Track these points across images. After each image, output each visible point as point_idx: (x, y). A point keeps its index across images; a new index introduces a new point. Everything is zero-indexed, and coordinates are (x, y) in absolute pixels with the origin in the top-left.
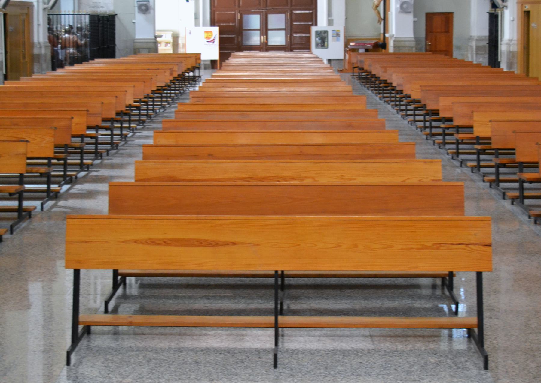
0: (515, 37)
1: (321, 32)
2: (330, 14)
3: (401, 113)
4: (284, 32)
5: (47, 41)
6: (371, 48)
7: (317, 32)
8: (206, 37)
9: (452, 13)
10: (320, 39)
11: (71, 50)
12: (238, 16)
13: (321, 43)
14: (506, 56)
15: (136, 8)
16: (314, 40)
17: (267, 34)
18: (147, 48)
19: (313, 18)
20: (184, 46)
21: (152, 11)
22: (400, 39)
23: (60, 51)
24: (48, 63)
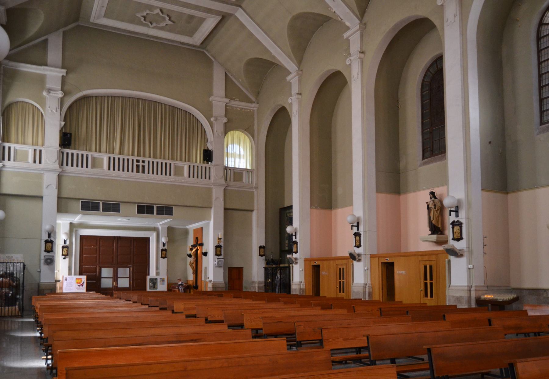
0: (303, 280)
1: (153, 279)
2: (157, 268)
7: (150, 279)
8: (77, 282)
9: (242, 268)
10: (152, 284)
12: (98, 269)
13: (153, 286)
17: (117, 281)
18: (50, 289)
19: (146, 271)
20: (61, 288)
21: (54, 263)
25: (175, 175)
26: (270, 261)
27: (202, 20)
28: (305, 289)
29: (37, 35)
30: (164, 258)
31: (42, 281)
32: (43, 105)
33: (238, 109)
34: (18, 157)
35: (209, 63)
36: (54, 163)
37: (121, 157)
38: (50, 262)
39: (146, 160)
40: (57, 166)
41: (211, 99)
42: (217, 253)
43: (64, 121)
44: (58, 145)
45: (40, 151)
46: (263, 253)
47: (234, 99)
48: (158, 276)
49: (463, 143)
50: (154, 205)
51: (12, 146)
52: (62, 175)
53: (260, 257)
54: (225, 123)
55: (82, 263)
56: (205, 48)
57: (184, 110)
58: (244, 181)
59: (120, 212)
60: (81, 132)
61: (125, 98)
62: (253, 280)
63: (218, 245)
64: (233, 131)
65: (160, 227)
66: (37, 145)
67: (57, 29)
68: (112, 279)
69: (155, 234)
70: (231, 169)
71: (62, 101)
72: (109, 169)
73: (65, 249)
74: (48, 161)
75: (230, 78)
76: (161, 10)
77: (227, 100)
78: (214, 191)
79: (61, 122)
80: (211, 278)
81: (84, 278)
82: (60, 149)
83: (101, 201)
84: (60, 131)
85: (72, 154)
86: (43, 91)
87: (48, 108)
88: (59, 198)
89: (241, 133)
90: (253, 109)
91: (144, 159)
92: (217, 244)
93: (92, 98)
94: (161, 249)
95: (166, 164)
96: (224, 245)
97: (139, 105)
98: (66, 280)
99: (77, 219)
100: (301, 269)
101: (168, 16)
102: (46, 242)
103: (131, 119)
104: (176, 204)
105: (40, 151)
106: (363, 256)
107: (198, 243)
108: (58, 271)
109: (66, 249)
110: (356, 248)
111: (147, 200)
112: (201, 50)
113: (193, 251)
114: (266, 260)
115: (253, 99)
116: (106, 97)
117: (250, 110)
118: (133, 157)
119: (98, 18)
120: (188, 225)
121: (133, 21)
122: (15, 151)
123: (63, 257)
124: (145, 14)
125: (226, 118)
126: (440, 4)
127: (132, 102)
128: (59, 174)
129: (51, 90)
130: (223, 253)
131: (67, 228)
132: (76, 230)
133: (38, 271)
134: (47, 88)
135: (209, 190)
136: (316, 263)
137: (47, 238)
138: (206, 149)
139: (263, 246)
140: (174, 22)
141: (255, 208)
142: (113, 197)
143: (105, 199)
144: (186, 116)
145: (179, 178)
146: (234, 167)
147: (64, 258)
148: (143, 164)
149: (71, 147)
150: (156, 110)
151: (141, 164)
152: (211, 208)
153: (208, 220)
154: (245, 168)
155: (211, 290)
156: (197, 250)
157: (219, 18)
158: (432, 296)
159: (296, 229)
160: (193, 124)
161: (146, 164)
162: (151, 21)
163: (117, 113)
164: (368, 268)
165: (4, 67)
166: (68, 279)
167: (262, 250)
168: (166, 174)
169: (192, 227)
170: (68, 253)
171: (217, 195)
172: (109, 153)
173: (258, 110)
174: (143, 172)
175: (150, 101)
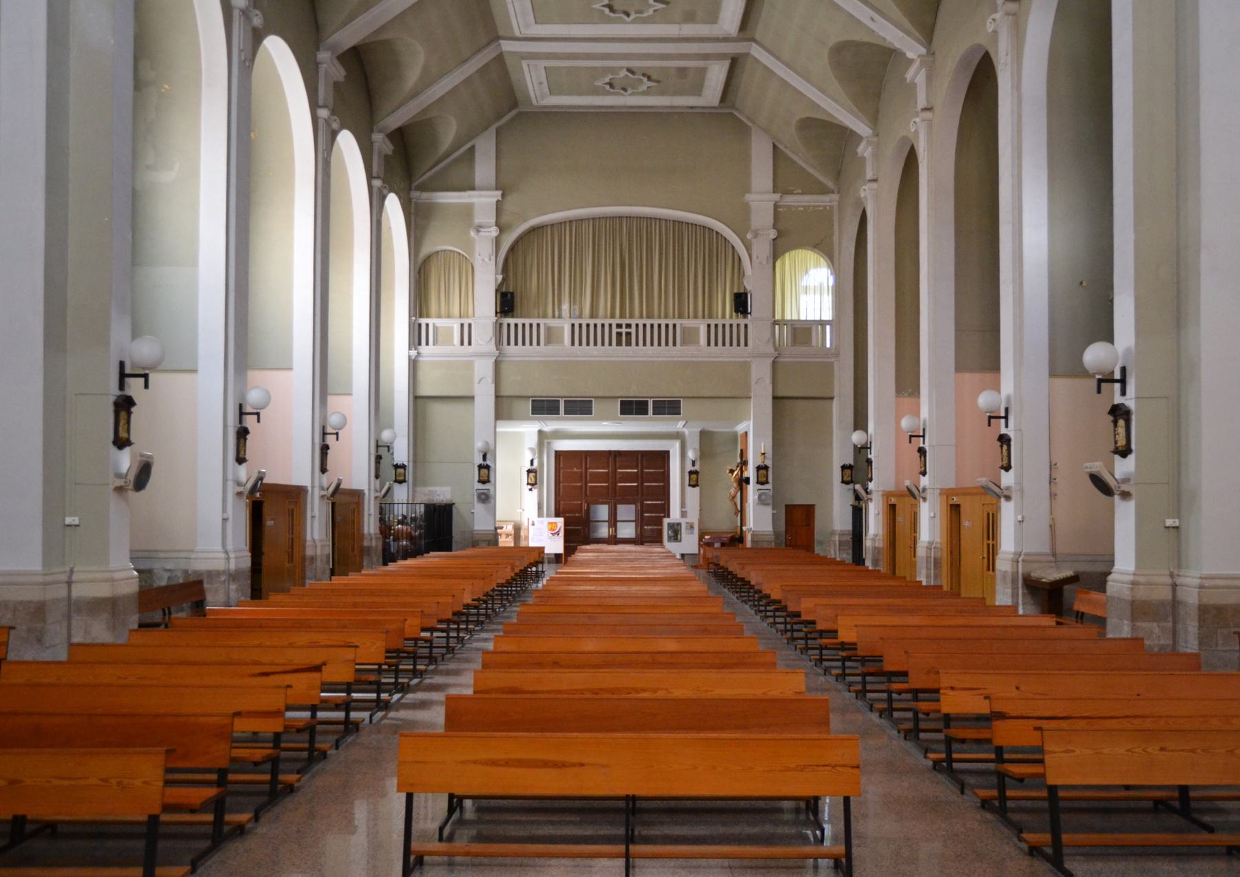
0: (881, 532)
1: (674, 524)
2: (683, 504)
5: (378, 531)
6: (728, 541)
7: (669, 524)
10: (672, 532)
11: (405, 543)
13: (674, 536)
14: (871, 552)
15: (476, 497)
16: (666, 533)
20: (527, 538)
21: (492, 501)
22: (758, 533)
25: (684, 343)
27: (702, 72)
29: (456, 146)
30: (694, 486)
32: (471, 252)
34: (440, 338)
35: (742, 131)
36: (488, 342)
37: (592, 322)
38: (486, 498)
39: (633, 322)
40: (492, 347)
41: (748, 197)
42: (760, 479)
45: (470, 325)
46: (849, 479)
47: (791, 193)
48: (683, 519)
50: (649, 399)
51: (430, 321)
52: (501, 361)
53: (844, 485)
54: (774, 240)
55: (559, 496)
57: (700, 226)
60: (530, 286)
63: (761, 464)
64: (793, 251)
66: (468, 317)
67: (486, 128)
68: (634, 523)
71: (498, 242)
73: (532, 475)
75: (782, 152)
76: (629, 70)
77: (777, 197)
78: (753, 367)
80: (752, 526)
81: (560, 521)
83: (562, 397)
85: (516, 325)
87: (479, 257)
88: (498, 397)
89: (810, 252)
93: (545, 229)
94: (689, 470)
95: (667, 326)
96: (773, 465)
97: (621, 228)
98: (533, 525)
101: (644, 75)
103: (610, 251)
104: (683, 395)
105: (470, 325)
109: (534, 474)
111: (634, 392)
113: (734, 475)
115: (830, 184)
117: (825, 207)
119: (543, 98)
121: (596, 92)
122: (435, 328)
123: (530, 487)
124: (607, 80)
125: (774, 230)
129: (481, 227)
130: (770, 479)
131: (532, 441)
132: (549, 443)
135: (745, 366)
136: (955, 500)
137: (481, 462)
138: (742, 291)
139: (850, 465)
140: (658, 82)
142: (579, 390)
143: (567, 395)
146: (797, 319)
147: (531, 490)
148: (628, 330)
150: (651, 233)
151: (624, 330)
152: (750, 398)
154: (818, 319)
161: (633, 330)
164: (934, 514)
167: (848, 472)
171: (761, 373)
174: (629, 344)
175: (640, 218)
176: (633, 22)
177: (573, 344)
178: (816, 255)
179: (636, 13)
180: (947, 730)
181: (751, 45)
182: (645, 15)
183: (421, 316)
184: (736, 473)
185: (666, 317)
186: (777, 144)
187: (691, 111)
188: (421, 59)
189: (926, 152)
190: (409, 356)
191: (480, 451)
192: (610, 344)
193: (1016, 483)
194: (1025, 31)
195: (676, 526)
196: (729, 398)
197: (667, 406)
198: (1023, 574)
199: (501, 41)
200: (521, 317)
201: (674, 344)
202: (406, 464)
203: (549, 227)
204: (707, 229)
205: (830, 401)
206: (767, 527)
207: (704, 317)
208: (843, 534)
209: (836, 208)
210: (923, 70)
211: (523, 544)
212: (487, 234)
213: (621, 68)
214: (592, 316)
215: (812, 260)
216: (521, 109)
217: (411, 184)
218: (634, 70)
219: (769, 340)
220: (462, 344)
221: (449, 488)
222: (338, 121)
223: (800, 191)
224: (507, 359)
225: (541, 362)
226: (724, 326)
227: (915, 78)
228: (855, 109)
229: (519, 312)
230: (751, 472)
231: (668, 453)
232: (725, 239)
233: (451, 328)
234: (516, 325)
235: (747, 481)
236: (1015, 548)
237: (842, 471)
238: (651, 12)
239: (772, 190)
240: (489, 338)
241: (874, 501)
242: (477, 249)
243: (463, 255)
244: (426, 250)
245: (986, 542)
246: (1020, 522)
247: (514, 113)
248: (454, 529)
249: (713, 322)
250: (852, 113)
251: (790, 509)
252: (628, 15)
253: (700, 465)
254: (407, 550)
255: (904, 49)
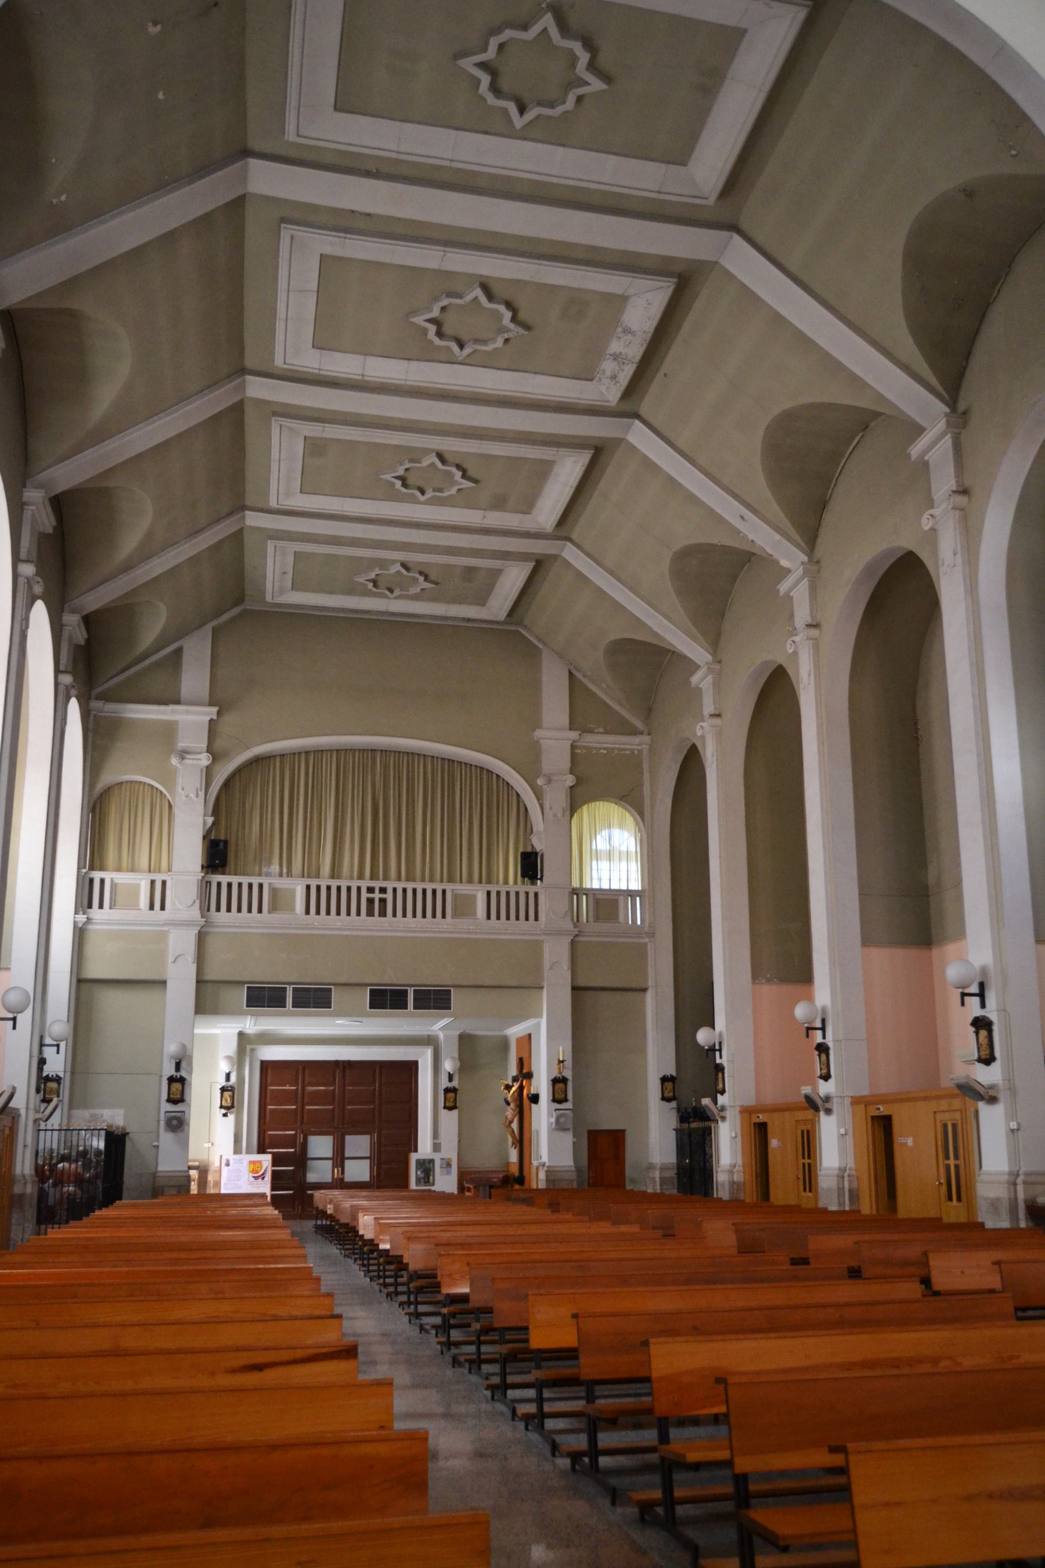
0: (740, 1162)
1: (424, 1161)
3: (385, 1291)
4: (368, 1162)
5: (33, 1172)
6: (499, 1184)
7: (418, 1161)
9: (623, 1132)
10: (422, 1172)
11: (71, 1188)
13: (424, 1178)
14: (727, 1188)
15: (162, 1123)
16: (413, 1173)
18: (176, 1186)
19: (411, 1143)
20: (218, 1184)
21: (186, 1128)
22: (556, 1169)
23: (52, 1191)
24: (31, 1213)
25: (455, 915)
26: (689, 1113)
27: (495, 575)
28: (744, 1182)
30: (450, 1109)
31: (160, 1169)
32: (170, 784)
33: (602, 751)
34: (120, 898)
35: (531, 654)
37: (334, 883)
38: (178, 1124)
39: (389, 885)
40: (195, 913)
41: (538, 733)
42: (557, 1096)
43: (212, 816)
44: (199, 868)
45: (164, 883)
46: (671, 1094)
47: (590, 731)
48: (436, 1154)
49: (984, 836)
51: (107, 876)
52: (206, 933)
54: (571, 788)
56: (520, 623)
57: (476, 766)
58: (621, 918)
59: (330, 1007)
60: (250, 832)
61: (343, 753)
62: (650, 1161)
63: (559, 1075)
65: (441, 1036)
66: (160, 872)
68: (330, 1162)
69: (429, 1052)
70: (588, 892)
71: (209, 773)
72: (308, 912)
73: (227, 1094)
74: (178, 904)
75: (580, 682)
76: (404, 565)
77: (574, 735)
79: (206, 818)
80: (545, 1158)
81: (266, 1159)
82: (203, 877)
83: (290, 984)
84: (204, 837)
85: (230, 885)
86: (169, 758)
87: (180, 791)
89: (613, 805)
90: (639, 747)
91: (384, 884)
92: (555, 1074)
94: (444, 1087)
95: (434, 892)
96: (573, 1076)
99: (251, 1025)
100: (842, 1131)
101: (421, 573)
102: (171, 1080)
103: (358, 796)
104: (456, 983)
105: (164, 883)
106: (835, 1100)
107: (525, 1074)
108: (212, 1144)
109: (230, 1093)
110: (980, 1067)
111: (391, 977)
112: (513, 628)
113: (512, 1092)
114: (679, 1110)
115: (639, 724)
116: (303, 754)
117: (632, 750)
118: (360, 883)
119: (281, 592)
120: (508, 1028)
121: (352, 590)
123: (223, 1111)
126: (927, 528)
127: (359, 758)
128: (199, 931)
129: (188, 753)
131: (230, 1047)
132: (252, 1050)
133: (154, 1146)
134: (179, 748)
136: (882, 1110)
138: (529, 850)
140: (437, 583)
141: (650, 984)
142: (314, 975)
144: (481, 779)
145: (464, 923)
146: (608, 888)
147: (225, 1115)
148: (383, 896)
149: (227, 869)
151: (377, 896)
152: (542, 988)
153: (535, 1017)
155: (544, 1187)
156: (521, 1088)
157: (530, 566)
158: (959, 1199)
159: (720, 1035)
160: (498, 796)
161: (389, 896)
162: (389, 586)
163: (326, 786)
164: (846, 1130)
165: (95, 716)
166: (231, 1163)
167: (669, 1085)
168: (434, 916)
169: (515, 1031)
170: (233, 1103)
172: (309, 877)
173: (650, 750)
174: (383, 913)
175: (398, 753)
176: (427, 503)
177: (308, 912)
178: (620, 808)
179: (434, 491)
180: (664, 1447)
181: (566, 544)
182: (445, 494)
183: (92, 868)
184: (514, 1089)
185: (432, 880)
186: (574, 672)
187: (465, 624)
188: (145, 523)
189: (812, 677)
190: (75, 923)
191: (172, 1057)
192: (358, 914)
193: (1003, 1080)
194: (980, 531)
195: (427, 1165)
196: (515, 987)
197: (432, 996)
198: (1026, 1201)
199: (247, 513)
200: (236, 874)
201: (444, 916)
202: (61, 1075)
203: (278, 760)
204: (485, 770)
205: (642, 993)
206: (566, 1161)
207: (480, 882)
208: (665, 1169)
209: (645, 752)
210: (806, 579)
211: (211, 1190)
212: (195, 762)
213: (394, 562)
214: (333, 876)
215: (616, 816)
216: (248, 606)
217: (90, 690)
218: (410, 565)
219: (566, 912)
220: (152, 907)
221: (122, 1112)
222: (42, 584)
223: (602, 730)
224: (212, 930)
225: (262, 934)
226: (508, 893)
227: (791, 591)
228: (694, 630)
229: (232, 867)
230: (541, 1084)
231: (416, 1063)
232: (508, 784)
233: (137, 887)
234: (230, 885)
235: (535, 1099)
236: (1009, 1167)
237: (662, 1084)
238: (453, 491)
239: (568, 726)
240: (192, 901)
241: (728, 1119)
242: (180, 780)
243: (157, 789)
244: (107, 778)
245: (961, 1162)
246: (1013, 1131)
247: (235, 611)
248: (126, 1170)
249: (494, 889)
250: (686, 632)
251: (595, 1137)
252: (423, 492)
253: (460, 1078)
254: (75, 1199)
255: (776, 556)
